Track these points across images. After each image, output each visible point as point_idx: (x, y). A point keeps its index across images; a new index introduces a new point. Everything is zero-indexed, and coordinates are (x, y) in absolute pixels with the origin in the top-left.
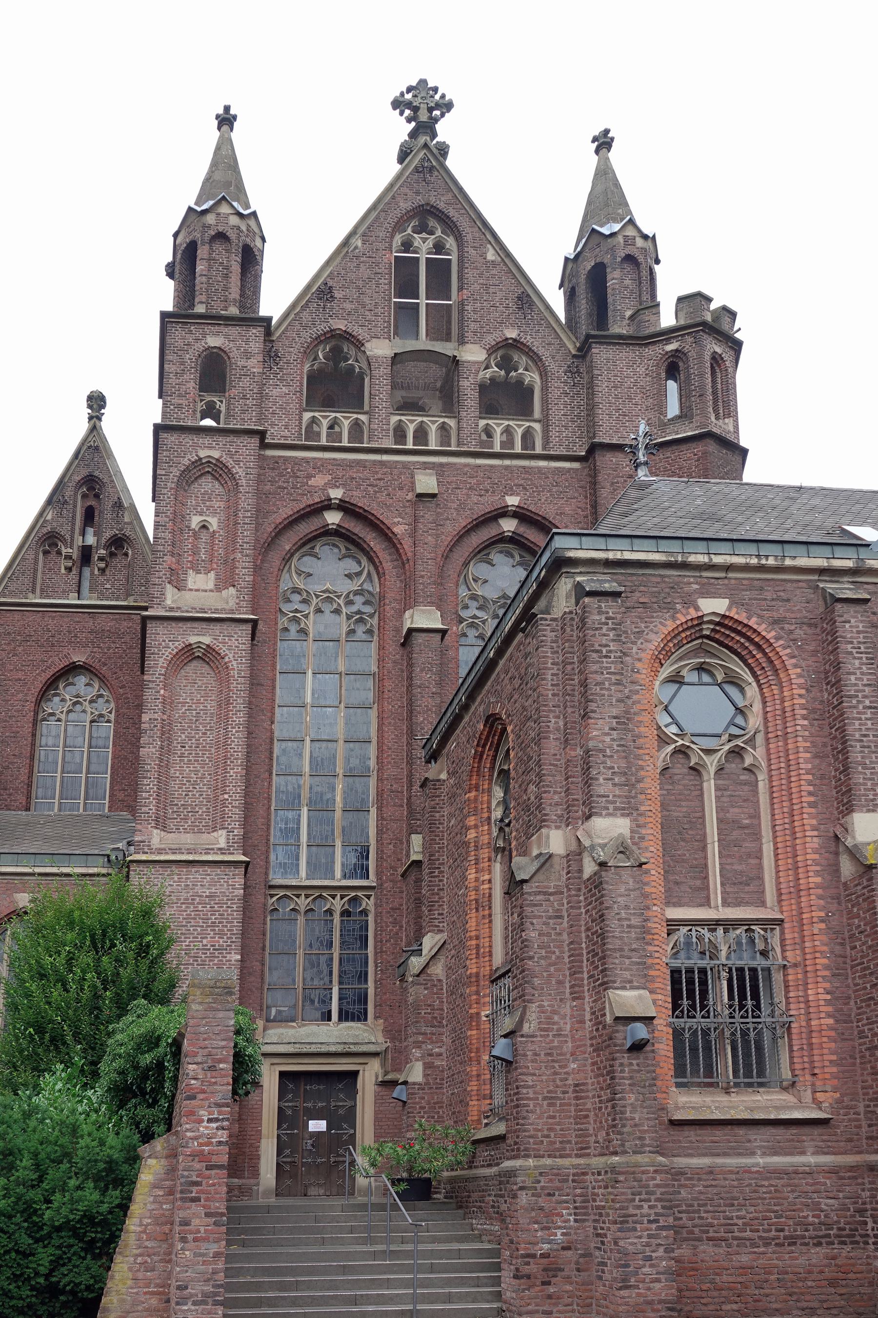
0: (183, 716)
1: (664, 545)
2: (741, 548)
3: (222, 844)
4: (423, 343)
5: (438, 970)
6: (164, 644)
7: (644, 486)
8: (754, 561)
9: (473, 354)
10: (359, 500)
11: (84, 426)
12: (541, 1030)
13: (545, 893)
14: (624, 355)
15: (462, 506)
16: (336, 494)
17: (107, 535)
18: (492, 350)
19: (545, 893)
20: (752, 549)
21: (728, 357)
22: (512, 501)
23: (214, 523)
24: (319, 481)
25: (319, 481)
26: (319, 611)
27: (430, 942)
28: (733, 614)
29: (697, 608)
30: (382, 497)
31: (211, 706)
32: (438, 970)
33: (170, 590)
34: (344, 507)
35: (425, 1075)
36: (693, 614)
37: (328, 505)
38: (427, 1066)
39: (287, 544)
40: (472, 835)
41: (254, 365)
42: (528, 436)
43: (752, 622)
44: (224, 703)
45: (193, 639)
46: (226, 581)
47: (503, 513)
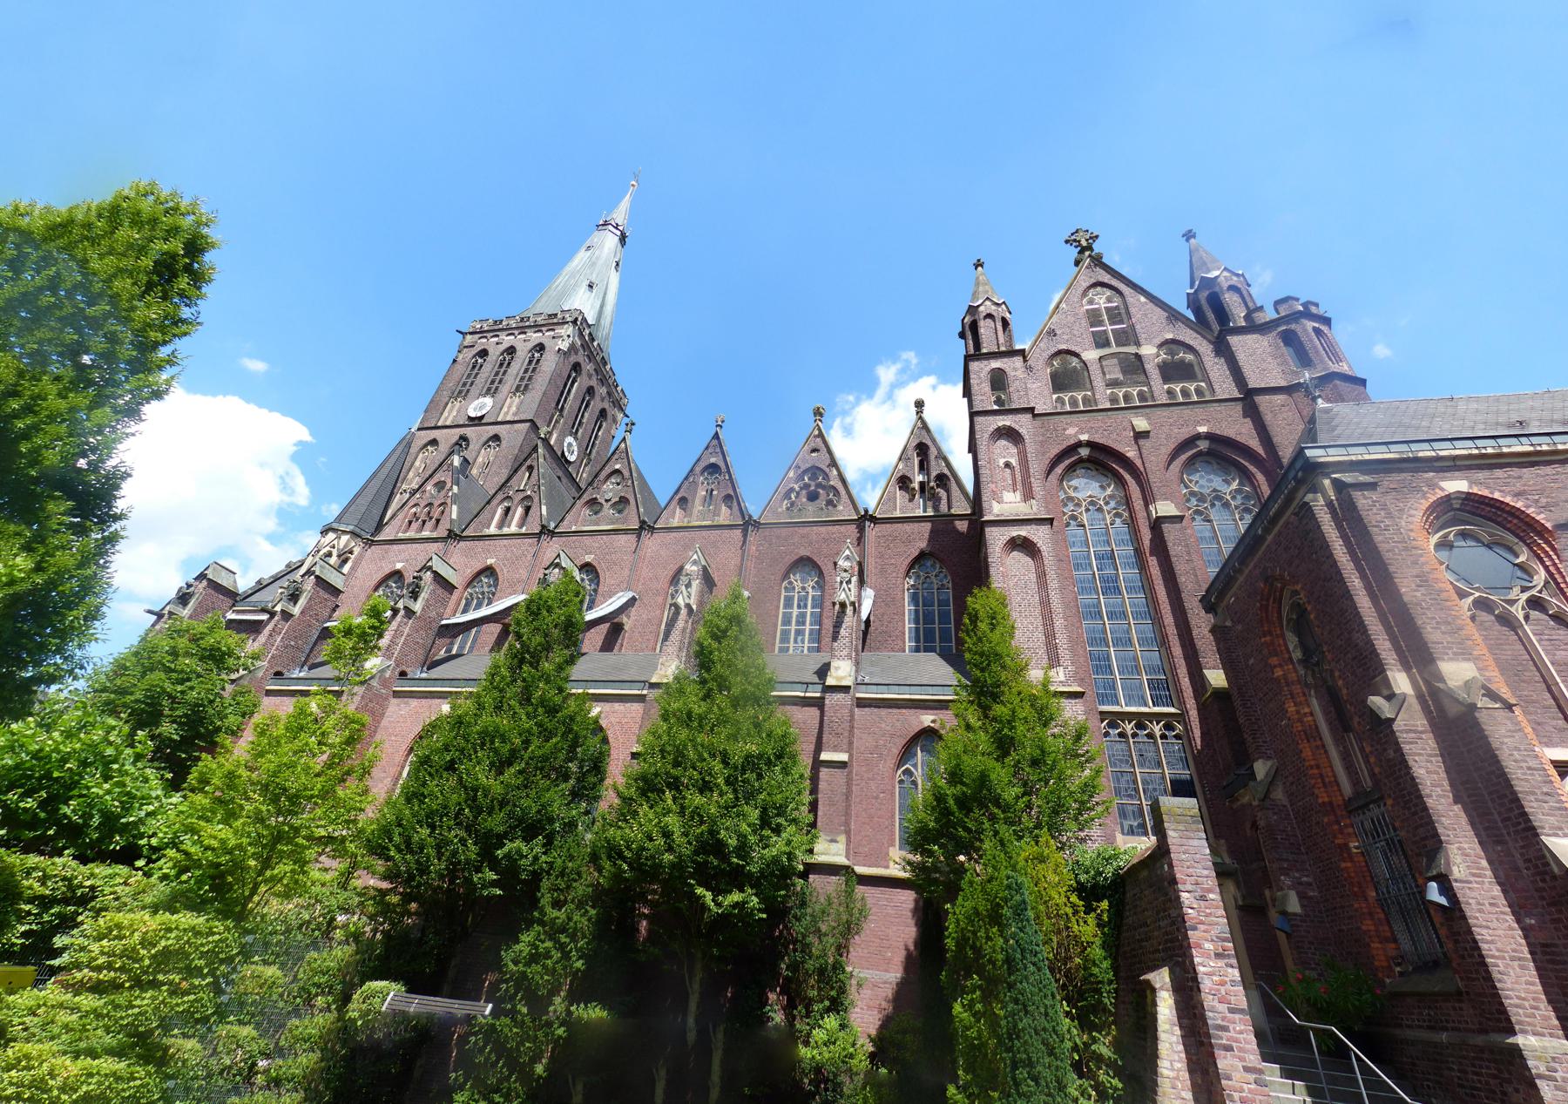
0: (1016, 584)
1: (1393, 448)
2: (1458, 444)
3: (1062, 678)
4: (1114, 349)
5: (1279, 794)
6: (996, 539)
7: (1327, 411)
8: (1476, 452)
9: (1148, 350)
10: (1099, 439)
11: (914, 417)
12: (1474, 875)
13: (1415, 732)
14: (1250, 339)
15: (1168, 437)
16: (1084, 437)
17: (934, 474)
18: (1160, 346)
19: (1415, 732)
20: (1469, 443)
21: (1324, 328)
22: (1203, 429)
23: (1014, 461)
24: (1071, 431)
25: (1071, 431)
26: (1087, 510)
27: (1261, 769)
28: (1475, 490)
29: (1442, 489)
30: (1114, 436)
31: (1033, 577)
32: (1279, 794)
33: (995, 504)
34: (1089, 444)
35: (1302, 906)
36: (1440, 494)
37: (1080, 444)
38: (1302, 897)
39: (1059, 470)
40: (1278, 673)
41: (1020, 374)
42: (1199, 392)
43: (1497, 495)
44: (1042, 576)
45: (1015, 534)
46: (1028, 495)
47: (1198, 436)
